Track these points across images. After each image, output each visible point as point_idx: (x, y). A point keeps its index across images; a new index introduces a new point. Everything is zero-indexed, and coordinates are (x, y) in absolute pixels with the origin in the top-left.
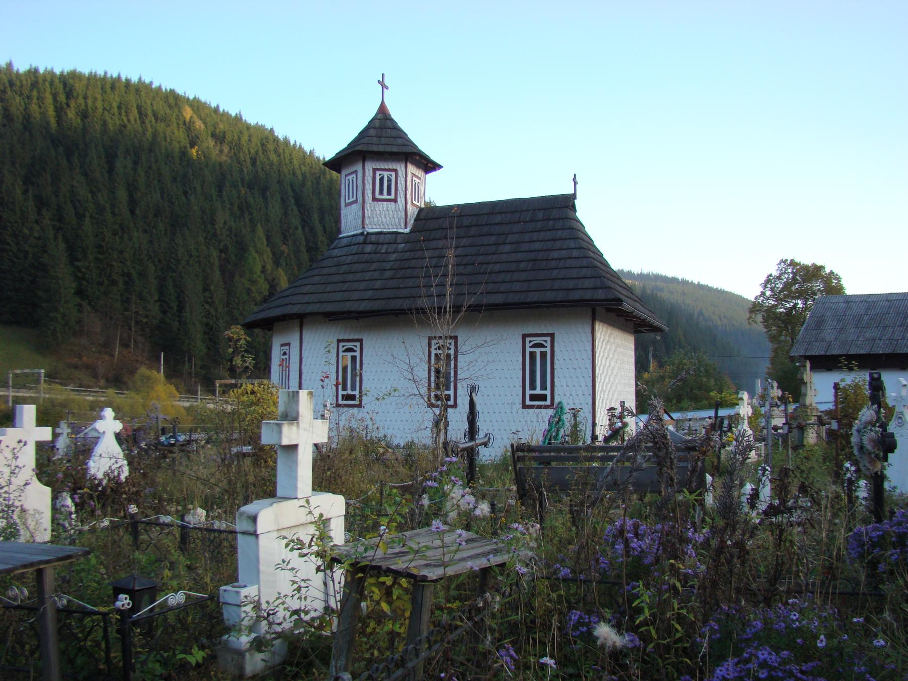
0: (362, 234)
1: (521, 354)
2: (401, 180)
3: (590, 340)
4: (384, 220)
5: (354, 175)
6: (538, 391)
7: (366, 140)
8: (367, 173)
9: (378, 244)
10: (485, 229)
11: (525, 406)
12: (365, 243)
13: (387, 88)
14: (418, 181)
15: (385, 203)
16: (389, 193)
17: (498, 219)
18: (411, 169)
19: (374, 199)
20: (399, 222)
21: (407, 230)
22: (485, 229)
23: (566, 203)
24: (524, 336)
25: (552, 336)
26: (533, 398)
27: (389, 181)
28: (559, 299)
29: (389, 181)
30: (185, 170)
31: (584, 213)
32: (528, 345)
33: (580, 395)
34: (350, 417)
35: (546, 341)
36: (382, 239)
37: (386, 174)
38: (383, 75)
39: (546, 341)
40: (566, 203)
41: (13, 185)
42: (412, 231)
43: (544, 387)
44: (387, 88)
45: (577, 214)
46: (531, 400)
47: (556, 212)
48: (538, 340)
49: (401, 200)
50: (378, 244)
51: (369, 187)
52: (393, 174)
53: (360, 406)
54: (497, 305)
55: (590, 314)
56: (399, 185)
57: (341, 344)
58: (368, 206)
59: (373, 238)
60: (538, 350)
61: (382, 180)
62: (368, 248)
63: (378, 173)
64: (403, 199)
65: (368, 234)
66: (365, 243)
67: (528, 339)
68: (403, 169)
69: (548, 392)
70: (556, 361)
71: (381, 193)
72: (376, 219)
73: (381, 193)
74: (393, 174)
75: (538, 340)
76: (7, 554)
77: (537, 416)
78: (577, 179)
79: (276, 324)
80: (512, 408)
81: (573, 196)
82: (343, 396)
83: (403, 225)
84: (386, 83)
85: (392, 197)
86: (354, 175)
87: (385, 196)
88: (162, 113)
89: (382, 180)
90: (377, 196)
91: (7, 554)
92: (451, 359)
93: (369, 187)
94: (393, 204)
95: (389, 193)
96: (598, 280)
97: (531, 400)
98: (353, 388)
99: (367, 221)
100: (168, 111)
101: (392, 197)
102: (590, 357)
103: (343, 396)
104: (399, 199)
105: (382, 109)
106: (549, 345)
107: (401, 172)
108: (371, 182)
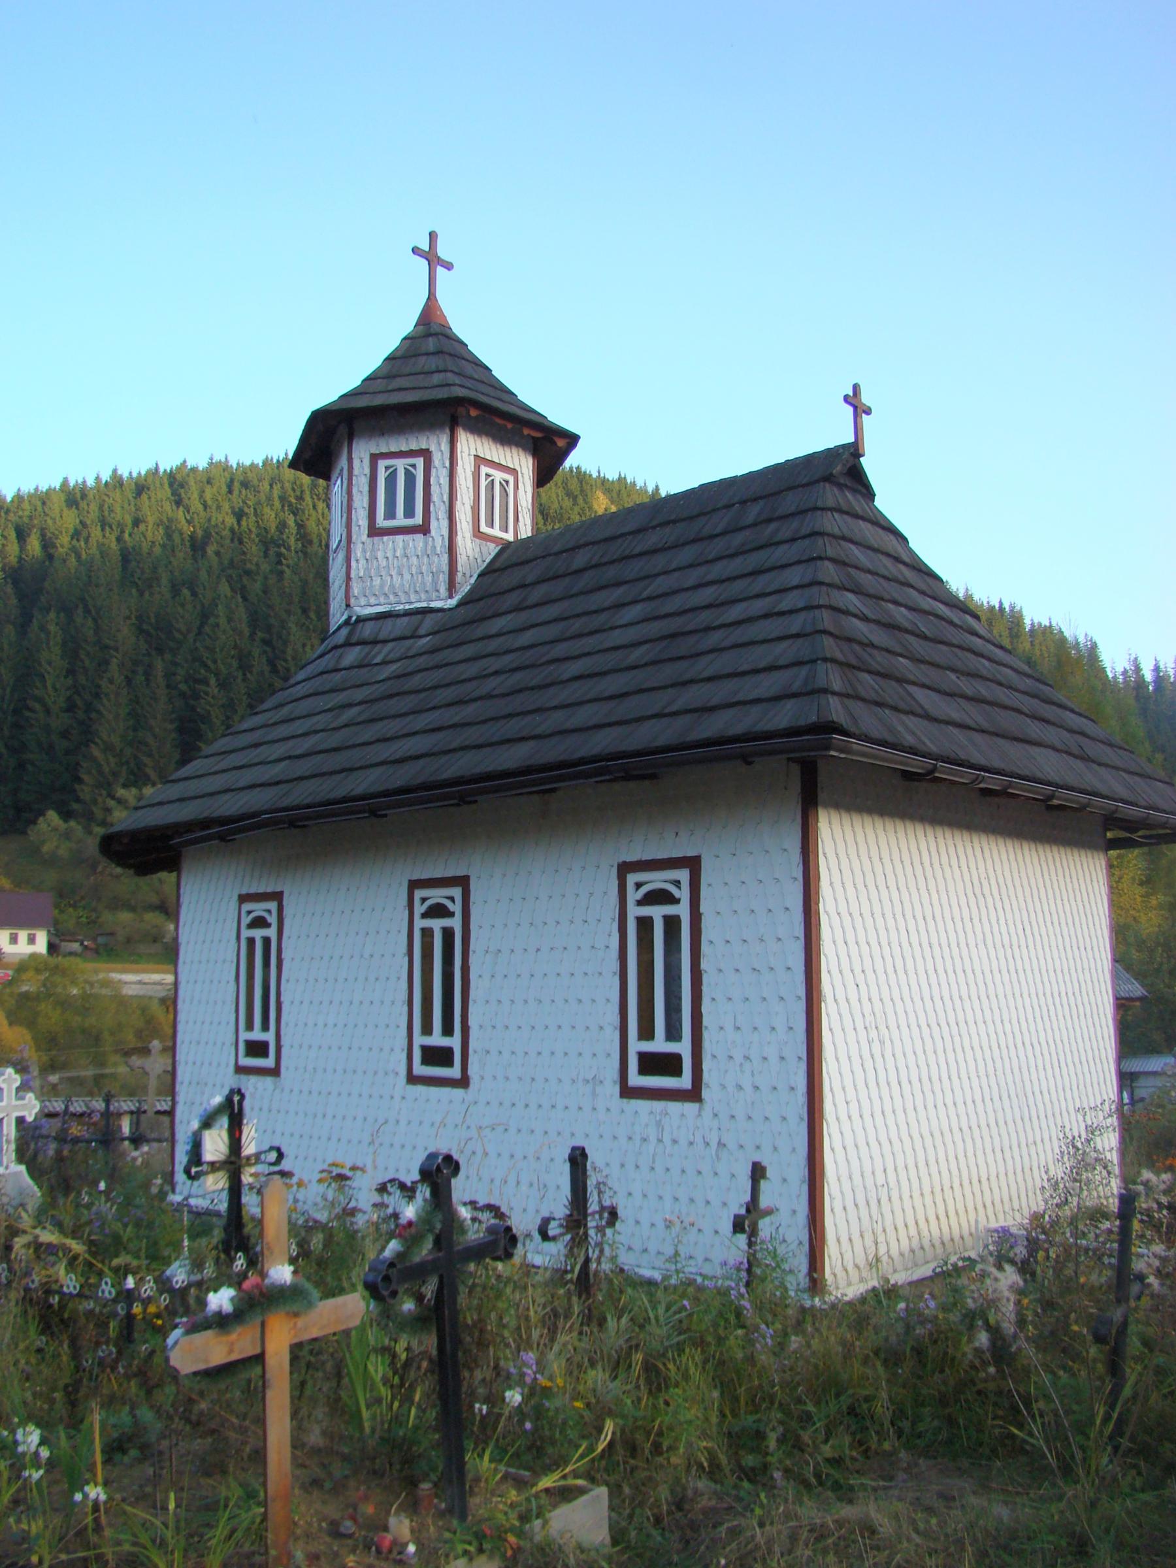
0: (347, 622)
1: (616, 925)
2: (440, 476)
3: (799, 873)
4: (397, 581)
6: (659, 1045)
8: (356, 472)
9: (375, 642)
10: (611, 573)
11: (628, 1092)
12: (348, 644)
13: (846, 399)
14: (498, 476)
15: (399, 539)
16: (409, 512)
17: (652, 539)
18: (469, 445)
19: (375, 531)
20: (435, 582)
21: (452, 603)
22: (611, 573)
23: (842, 471)
24: (625, 869)
26: (653, 1064)
27: (410, 478)
28: (660, 742)
29: (410, 478)
31: (900, 493)
33: (773, 1059)
35: (677, 883)
36: (388, 629)
37: (401, 464)
39: (677, 883)
40: (842, 471)
41: (304, 645)
42: (460, 604)
44: (449, 266)
45: (879, 503)
46: (644, 1070)
47: (814, 504)
48: (657, 880)
49: (439, 527)
50: (375, 642)
51: (361, 502)
52: (420, 462)
53: (694, 1094)
56: (434, 489)
57: (419, 894)
58: (358, 551)
59: (367, 631)
60: (657, 913)
61: (391, 480)
62: (352, 656)
64: (445, 523)
65: (361, 620)
66: (348, 644)
67: (632, 879)
68: (445, 447)
69: (684, 1048)
70: (705, 948)
72: (377, 582)
75: (657, 880)
77: (658, 1123)
78: (866, 398)
80: (594, 1094)
81: (854, 451)
83: (443, 591)
84: (442, 252)
85: (418, 520)
87: (400, 521)
88: (556, 506)
89: (391, 480)
90: (381, 522)
93: (361, 502)
94: (419, 537)
95: (409, 513)
96: (804, 671)
97: (644, 1070)
98: (673, 1034)
99: (356, 590)
100: (567, 503)
101: (418, 520)
102: (800, 931)
104: (433, 525)
106: (684, 894)
107: (440, 458)
108: (366, 489)
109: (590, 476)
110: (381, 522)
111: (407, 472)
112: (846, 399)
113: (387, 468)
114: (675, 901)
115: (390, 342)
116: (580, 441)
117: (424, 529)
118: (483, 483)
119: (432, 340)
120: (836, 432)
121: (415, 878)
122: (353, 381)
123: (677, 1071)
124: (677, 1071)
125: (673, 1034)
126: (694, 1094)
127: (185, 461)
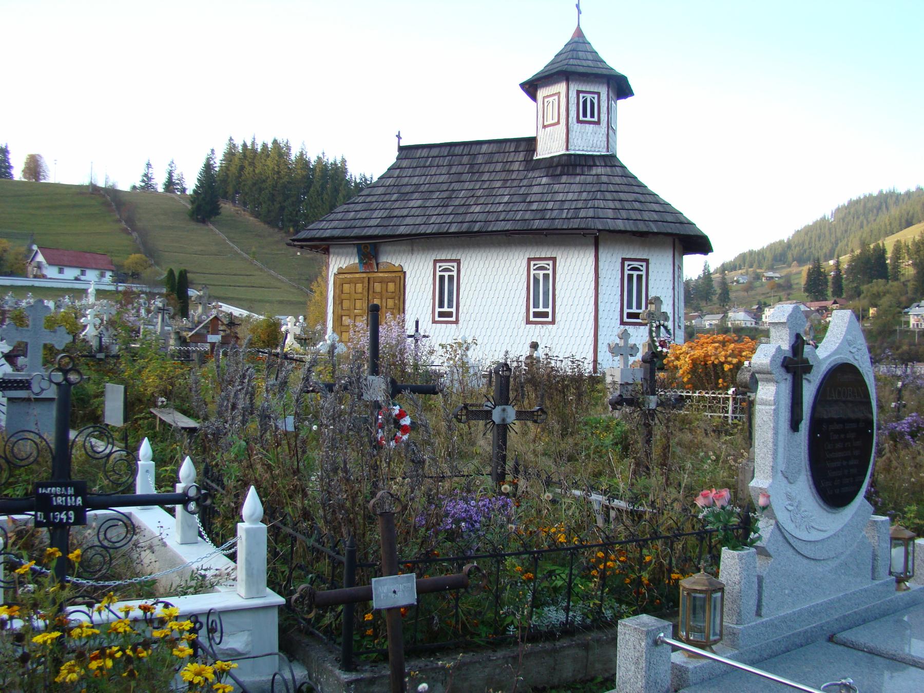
5: (556, 97)
6: (446, 309)
13: (620, 88)
16: (592, 116)
19: (579, 121)
24: (436, 261)
25: (458, 262)
26: (536, 315)
32: (626, 268)
34: (536, 333)
37: (589, 96)
43: (546, 305)
48: (636, 264)
52: (596, 96)
54: (519, 234)
55: (593, 241)
60: (635, 273)
61: (585, 102)
63: (581, 95)
69: (550, 310)
71: (585, 115)
73: (585, 115)
75: (636, 264)
79: (382, 248)
82: (628, 314)
85: (596, 119)
86: (556, 97)
87: (588, 118)
89: (585, 102)
90: (581, 118)
92: (550, 280)
95: (592, 116)
98: (450, 306)
101: (596, 119)
103: (628, 314)
105: (579, 33)
106: (644, 269)
109: (310, 162)
114: (452, 271)
115: (559, 47)
116: (629, 99)
117: (598, 123)
119: (578, 43)
120: (533, 135)
121: (624, 256)
123: (452, 316)
124: (452, 316)
125: (450, 306)
126: (457, 322)
127: (231, 139)
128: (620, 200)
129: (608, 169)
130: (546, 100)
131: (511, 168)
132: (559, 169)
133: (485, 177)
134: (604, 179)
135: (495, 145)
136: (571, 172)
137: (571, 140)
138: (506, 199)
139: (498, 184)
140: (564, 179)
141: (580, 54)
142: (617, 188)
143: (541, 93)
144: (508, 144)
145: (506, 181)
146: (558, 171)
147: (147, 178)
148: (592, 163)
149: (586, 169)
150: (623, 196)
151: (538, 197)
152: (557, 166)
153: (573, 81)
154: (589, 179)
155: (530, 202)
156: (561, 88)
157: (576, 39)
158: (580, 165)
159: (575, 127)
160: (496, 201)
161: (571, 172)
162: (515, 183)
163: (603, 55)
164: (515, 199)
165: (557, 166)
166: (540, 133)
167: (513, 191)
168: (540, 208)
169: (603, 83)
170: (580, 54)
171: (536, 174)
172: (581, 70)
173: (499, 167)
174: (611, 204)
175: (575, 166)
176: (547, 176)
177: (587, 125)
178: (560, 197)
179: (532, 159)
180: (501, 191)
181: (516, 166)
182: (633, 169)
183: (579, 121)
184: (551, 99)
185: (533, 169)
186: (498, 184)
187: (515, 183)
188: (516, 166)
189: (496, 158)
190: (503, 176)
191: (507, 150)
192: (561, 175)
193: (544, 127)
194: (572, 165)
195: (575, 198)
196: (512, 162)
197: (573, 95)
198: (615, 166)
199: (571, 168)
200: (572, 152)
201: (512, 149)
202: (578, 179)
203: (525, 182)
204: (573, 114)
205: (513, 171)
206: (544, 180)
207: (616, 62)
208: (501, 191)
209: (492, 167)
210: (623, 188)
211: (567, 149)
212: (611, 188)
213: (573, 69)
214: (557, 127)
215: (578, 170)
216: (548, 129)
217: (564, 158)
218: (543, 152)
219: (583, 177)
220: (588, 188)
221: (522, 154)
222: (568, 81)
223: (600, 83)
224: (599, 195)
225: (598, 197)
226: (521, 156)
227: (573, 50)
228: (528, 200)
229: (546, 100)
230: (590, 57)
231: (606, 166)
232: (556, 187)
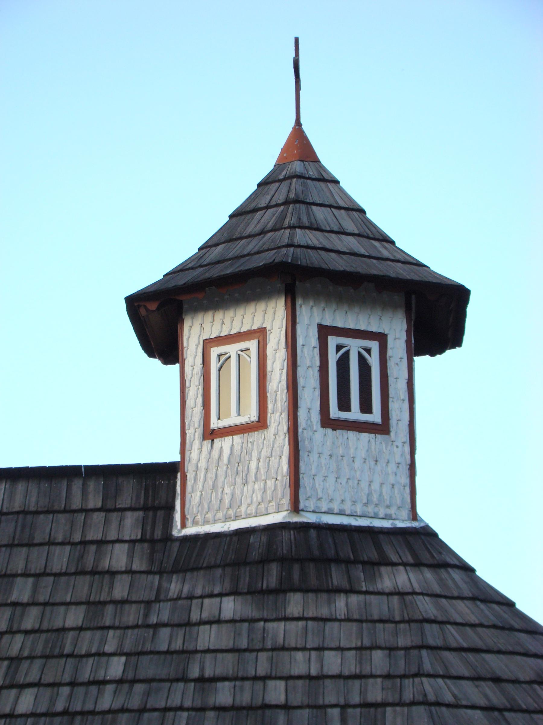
5: (252, 345)
7: (254, 224)
13: (436, 314)
16: (366, 407)
19: (327, 422)
30: (443, 284)
37: (354, 346)
38: (297, 40)
52: (374, 346)
63: (333, 341)
71: (344, 405)
73: (344, 405)
74: (374, 346)
76: (274, 217)
85: (376, 417)
86: (252, 345)
87: (355, 414)
90: (334, 412)
91: (274, 217)
95: (366, 407)
101: (376, 417)
105: (299, 146)
110: (334, 412)
111: (362, 359)
112: (436, 314)
113: (339, 348)
115: (241, 189)
117: (383, 428)
118: (333, 358)
119: (299, 179)
120: (162, 450)
122: (216, 220)
128: (497, 680)
129: (428, 574)
130: (214, 352)
131: (105, 564)
132: (274, 569)
133: (22, 591)
134: (426, 607)
135: (33, 487)
136: (313, 582)
137: (305, 480)
138: (116, 668)
139: (74, 617)
140: (295, 604)
141: (320, 214)
142: (473, 638)
143: (195, 332)
144: (77, 484)
145: (94, 606)
146: (272, 576)
147: (372, 644)
148: (374, 555)
149: (358, 572)
150: (496, 664)
151: (226, 664)
152: (264, 561)
153: (306, 297)
154: (378, 607)
155: (201, 679)
156: (270, 315)
157: (297, 167)
158: (337, 560)
159: (315, 435)
160: (86, 675)
161: (313, 582)
162: (132, 614)
163: (380, 216)
164: (148, 668)
165: (264, 561)
166: (193, 454)
167: (130, 641)
168: (245, 698)
169: (394, 307)
170: (320, 214)
171: (197, 584)
172: (340, 264)
173: (61, 559)
174: (472, 692)
175: (325, 561)
176: (234, 593)
177: (352, 435)
178: (299, 663)
179: (168, 538)
180: (87, 642)
181: (118, 557)
182: (492, 573)
183: (327, 422)
184: (232, 349)
185: (181, 568)
186: (74, 617)
187: (132, 614)
188: (118, 557)
189: (44, 527)
190: (82, 587)
191: (76, 503)
192: (283, 589)
193: (210, 434)
194: (313, 560)
195: (352, 668)
196: (101, 543)
197: (307, 338)
198: (446, 565)
199: (311, 568)
200: (311, 518)
201: (95, 501)
202: (341, 604)
203: (163, 612)
204: (310, 398)
205: (113, 573)
206: (230, 607)
207: (425, 234)
208: (87, 642)
209: (38, 559)
210: (491, 638)
211: (296, 508)
212: (455, 636)
213: (315, 259)
214: (256, 436)
215: (337, 576)
216: (225, 444)
217: (286, 536)
218: (208, 510)
219: (354, 599)
220: (383, 634)
221: (130, 518)
222: (291, 296)
223: (387, 306)
224: (428, 662)
225: (427, 667)
226: (130, 525)
227: (297, 201)
228: (195, 672)
229: (214, 352)
230: (350, 227)
231: (418, 564)
232: (278, 631)
